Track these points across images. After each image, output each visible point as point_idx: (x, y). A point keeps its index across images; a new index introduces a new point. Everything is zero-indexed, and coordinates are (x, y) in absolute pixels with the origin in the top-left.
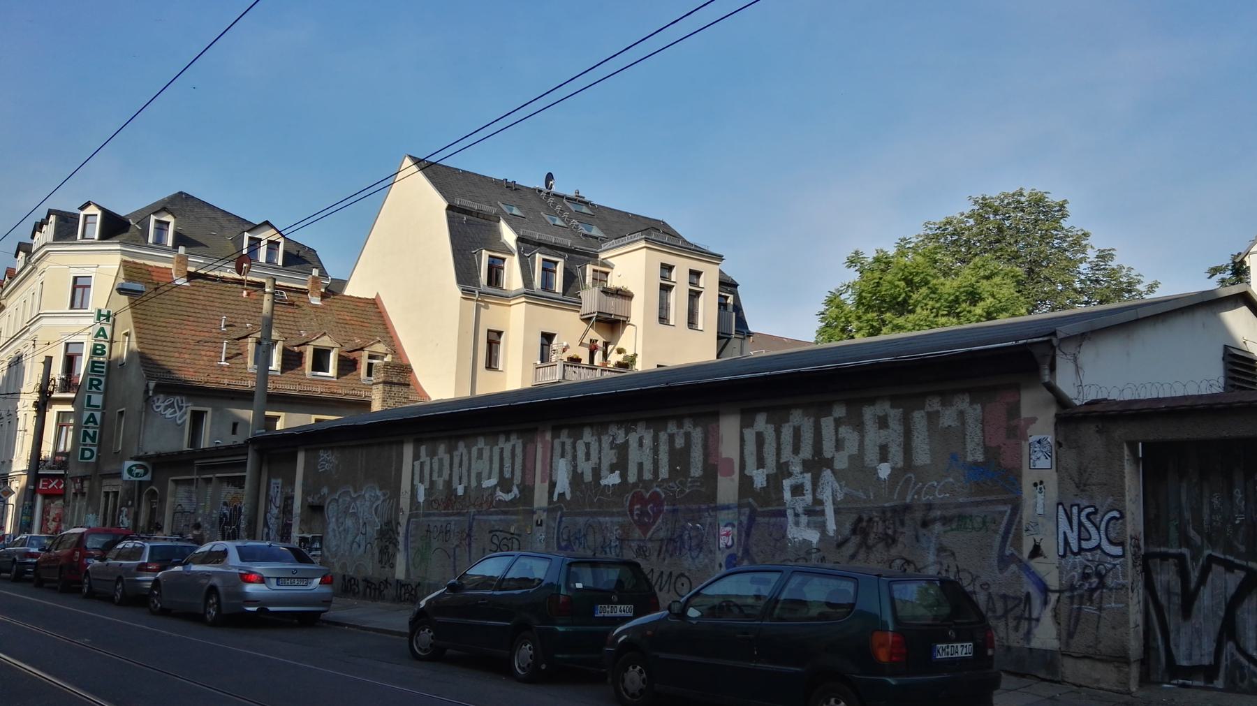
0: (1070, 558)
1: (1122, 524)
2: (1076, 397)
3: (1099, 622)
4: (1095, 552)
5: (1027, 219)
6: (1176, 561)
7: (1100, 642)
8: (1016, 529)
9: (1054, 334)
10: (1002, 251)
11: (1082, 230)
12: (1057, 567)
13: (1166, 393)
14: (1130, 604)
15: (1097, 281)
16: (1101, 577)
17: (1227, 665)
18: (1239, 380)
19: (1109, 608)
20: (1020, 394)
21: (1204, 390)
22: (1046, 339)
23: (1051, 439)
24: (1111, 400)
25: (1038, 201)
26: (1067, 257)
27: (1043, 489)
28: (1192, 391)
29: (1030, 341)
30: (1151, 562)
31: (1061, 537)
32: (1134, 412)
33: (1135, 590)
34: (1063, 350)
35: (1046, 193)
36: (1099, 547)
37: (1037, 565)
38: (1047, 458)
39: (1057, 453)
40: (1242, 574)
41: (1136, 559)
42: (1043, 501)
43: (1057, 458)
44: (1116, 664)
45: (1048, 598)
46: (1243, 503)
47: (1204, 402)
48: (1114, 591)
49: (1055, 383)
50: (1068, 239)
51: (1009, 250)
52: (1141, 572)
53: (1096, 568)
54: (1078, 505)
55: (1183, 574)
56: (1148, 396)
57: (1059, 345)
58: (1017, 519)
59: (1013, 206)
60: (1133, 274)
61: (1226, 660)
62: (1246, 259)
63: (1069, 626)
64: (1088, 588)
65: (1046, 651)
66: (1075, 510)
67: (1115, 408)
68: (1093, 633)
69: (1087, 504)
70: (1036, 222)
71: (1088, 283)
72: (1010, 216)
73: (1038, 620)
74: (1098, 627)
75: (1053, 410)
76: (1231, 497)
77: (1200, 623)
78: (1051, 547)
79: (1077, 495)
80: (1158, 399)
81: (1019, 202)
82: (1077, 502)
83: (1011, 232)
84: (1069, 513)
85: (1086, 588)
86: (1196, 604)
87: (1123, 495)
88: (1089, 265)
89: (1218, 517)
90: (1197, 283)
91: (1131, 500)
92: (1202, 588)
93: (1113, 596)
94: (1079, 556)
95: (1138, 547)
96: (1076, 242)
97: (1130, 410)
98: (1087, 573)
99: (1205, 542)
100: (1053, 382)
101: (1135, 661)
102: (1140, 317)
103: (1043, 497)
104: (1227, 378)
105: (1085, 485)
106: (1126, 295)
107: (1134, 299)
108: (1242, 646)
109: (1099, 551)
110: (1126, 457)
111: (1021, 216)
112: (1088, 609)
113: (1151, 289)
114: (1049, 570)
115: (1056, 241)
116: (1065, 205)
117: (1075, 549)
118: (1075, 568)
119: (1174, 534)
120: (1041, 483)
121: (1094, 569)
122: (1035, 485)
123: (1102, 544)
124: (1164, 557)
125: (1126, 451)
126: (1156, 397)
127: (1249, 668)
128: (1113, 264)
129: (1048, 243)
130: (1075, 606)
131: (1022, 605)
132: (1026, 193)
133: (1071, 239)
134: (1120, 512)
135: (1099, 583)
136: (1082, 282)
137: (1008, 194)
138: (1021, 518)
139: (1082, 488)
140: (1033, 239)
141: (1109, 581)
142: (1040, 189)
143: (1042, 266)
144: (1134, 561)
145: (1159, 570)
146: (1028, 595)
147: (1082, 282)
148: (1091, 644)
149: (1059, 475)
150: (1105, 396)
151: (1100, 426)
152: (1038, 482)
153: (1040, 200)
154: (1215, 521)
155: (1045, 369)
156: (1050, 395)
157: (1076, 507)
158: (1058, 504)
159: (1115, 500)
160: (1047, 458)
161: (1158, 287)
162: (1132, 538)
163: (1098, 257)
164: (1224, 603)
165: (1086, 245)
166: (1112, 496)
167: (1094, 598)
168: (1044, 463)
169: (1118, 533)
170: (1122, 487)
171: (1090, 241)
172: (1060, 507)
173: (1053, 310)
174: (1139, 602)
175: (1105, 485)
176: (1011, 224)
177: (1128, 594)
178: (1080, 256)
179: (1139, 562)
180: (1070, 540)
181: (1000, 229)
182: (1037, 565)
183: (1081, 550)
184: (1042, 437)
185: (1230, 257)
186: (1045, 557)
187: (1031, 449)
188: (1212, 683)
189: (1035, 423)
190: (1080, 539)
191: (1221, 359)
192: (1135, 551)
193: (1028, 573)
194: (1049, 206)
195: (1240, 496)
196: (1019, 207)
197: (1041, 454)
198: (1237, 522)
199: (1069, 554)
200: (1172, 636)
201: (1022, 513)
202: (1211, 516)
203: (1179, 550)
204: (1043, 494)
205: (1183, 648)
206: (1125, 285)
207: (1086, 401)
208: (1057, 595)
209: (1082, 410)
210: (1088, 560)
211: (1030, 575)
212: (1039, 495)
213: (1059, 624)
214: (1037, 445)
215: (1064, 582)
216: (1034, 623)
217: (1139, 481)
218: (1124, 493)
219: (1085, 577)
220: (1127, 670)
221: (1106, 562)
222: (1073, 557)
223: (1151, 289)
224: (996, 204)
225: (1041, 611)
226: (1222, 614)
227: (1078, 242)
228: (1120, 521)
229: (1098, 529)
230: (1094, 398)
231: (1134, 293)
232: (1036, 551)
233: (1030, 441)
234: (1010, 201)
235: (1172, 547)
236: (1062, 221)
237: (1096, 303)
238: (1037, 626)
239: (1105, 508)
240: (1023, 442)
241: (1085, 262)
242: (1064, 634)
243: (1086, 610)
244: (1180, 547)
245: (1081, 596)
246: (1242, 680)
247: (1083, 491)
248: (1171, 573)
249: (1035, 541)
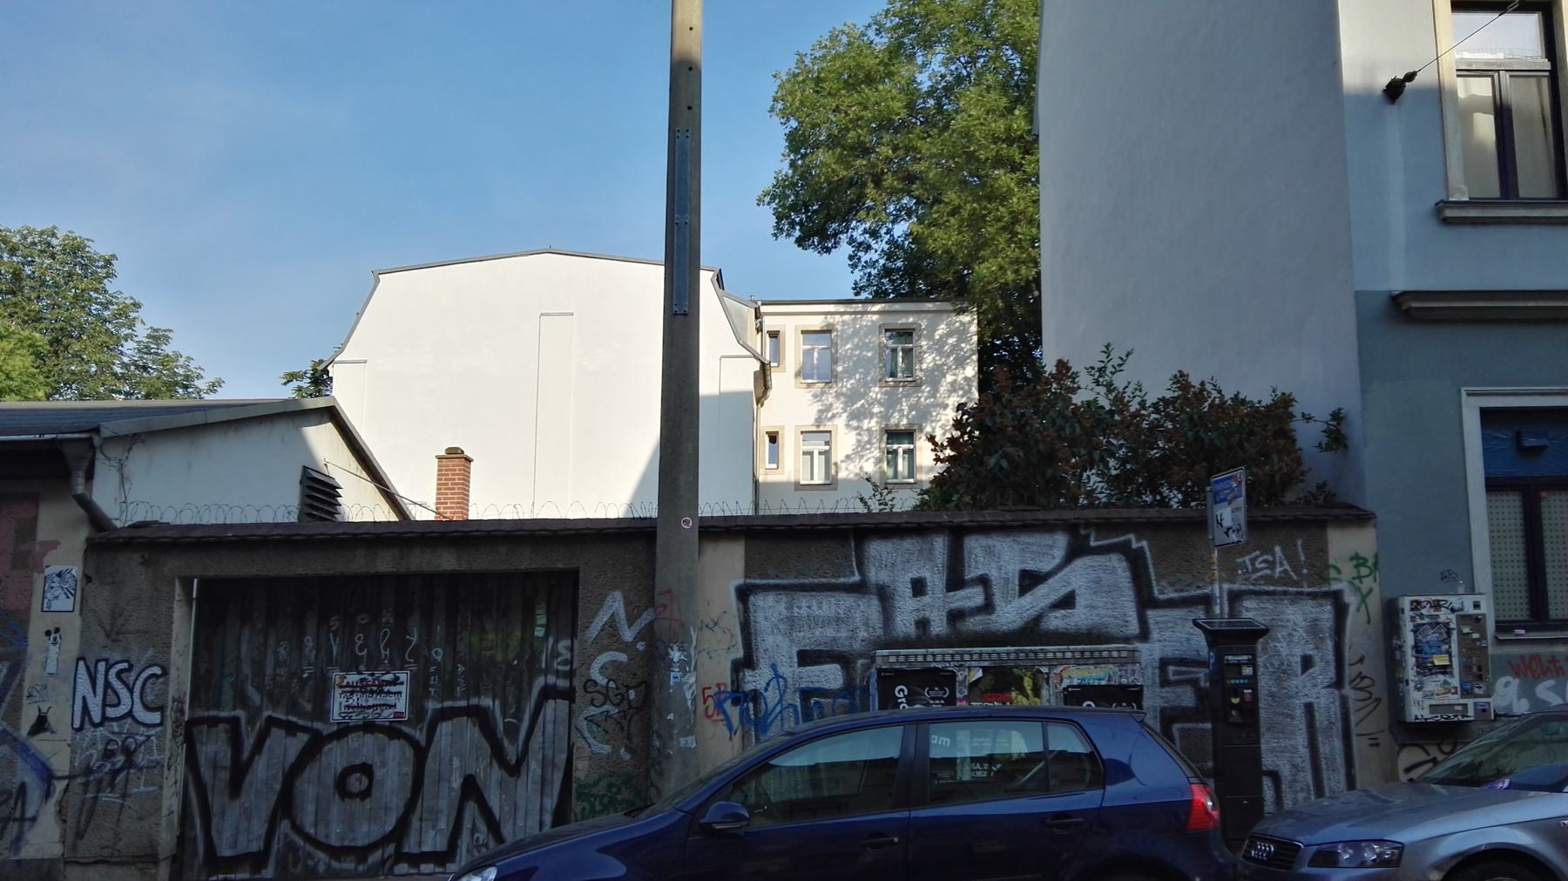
0: (89, 731)
1: (162, 683)
2: (116, 517)
3: (120, 814)
4: (124, 721)
5: (57, 270)
6: (227, 727)
7: (120, 840)
8: (12, 696)
9: (97, 430)
10: (15, 307)
11: (132, 298)
12: (69, 746)
13: (235, 518)
14: (165, 786)
15: (145, 368)
16: (129, 753)
17: (279, 849)
18: (317, 509)
19: (135, 793)
20: (37, 508)
21: (281, 518)
22: (84, 436)
23: (76, 572)
24: (162, 523)
25: (75, 249)
26: (107, 330)
27: (58, 639)
28: (267, 518)
29: (60, 436)
30: (195, 730)
31: (79, 703)
32: (572, 532)
33: (173, 767)
34: (105, 453)
35: (87, 240)
36: (130, 714)
37: (41, 744)
38: (68, 597)
39: (83, 590)
40: (304, 738)
41: (177, 727)
42: (57, 656)
43: (82, 598)
44: (140, 865)
45: (52, 788)
46: (314, 652)
47: (280, 532)
48: (145, 770)
49: (91, 496)
50: (111, 307)
51: (28, 308)
52: (182, 744)
53: (123, 742)
54: (106, 660)
55: (236, 741)
56: (213, 521)
57: (101, 447)
58: (17, 681)
59: (39, 247)
60: (192, 365)
61: (279, 843)
62: (329, 368)
63: (79, 822)
64: (110, 770)
65: (42, 860)
66: (102, 666)
67: (169, 533)
68: (112, 829)
69: (118, 658)
70: (69, 276)
71: (132, 368)
72: (33, 261)
73: (34, 819)
74: (118, 820)
75: (84, 533)
76: (300, 646)
77: (251, 802)
78: (62, 717)
79: (105, 647)
80: (225, 525)
81: (49, 244)
82: (104, 656)
83: (32, 283)
84: (92, 670)
85: (107, 770)
86: (249, 778)
87: (169, 647)
88: (135, 345)
89: (282, 671)
90: (274, 390)
91: (178, 652)
92: (257, 757)
93: (143, 777)
94: (101, 728)
95: (182, 711)
96: (122, 313)
97: (187, 537)
98: (110, 750)
99: (265, 700)
100: (88, 495)
101: (165, 859)
102: (209, 421)
103: (57, 650)
104: (303, 504)
105: (118, 633)
106: (181, 391)
107: (189, 397)
108: (298, 823)
109: (129, 720)
110: (177, 598)
111: (50, 265)
112: (107, 797)
113: (213, 388)
114: (58, 752)
115: (95, 306)
116: (113, 262)
117: (97, 719)
118: (94, 744)
119: (228, 694)
120: (57, 630)
121: (120, 743)
122: (48, 633)
123: (134, 710)
124: (213, 722)
125: (178, 590)
126: (221, 522)
127: (304, 848)
128: (168, 349)
129: (83, 307)
130: (90, 795)
131: (12, 802)
132: (61, 234)
133: (115, 307)
134: (163, 668)
135: (126, 762)
136: (124, 365)
137: (34, 230)
138: (22, 680)
139: (114, 636)
140: (64, 298)
141: (140, 759)
142: (80, 232)
143: (72, 337)
144: (174, 731)
145: (205, 738)
146: (23, 788)
147: (124, 365)
148: (108, 843)
149: (83, 621)
150: (156, 517)
151: (146, 556)
152: (52, 630)
153: (78, 248)
154: (278, 675)
155: (79, 476)
156: (81, 511)
157: (103, 663)
158: (78, 659)
159: (157, 653)
160: (68, 597)
161: (220, 386)
162: (174, 700)
163: (149, 336)
164: (281, 774)
165: (135, 318)
166: (154, 647)
167: (116, 782)
168: (65, 603)
169: (157, 695)
170: (169, 635)
171: (141, 314)
172: (81, 663)
173: (82, 396)
174: (176, 783)
175: (146, 633)
176: (34, 272)
177: (162, 773)
178: (125, 331)
179: (181, 730)
180: (91, 707)
181: (17, 276)
182: (41, 744)
183: (105, 719)
184: (63, 568)
185: (311, 364)
186: (53, 732)
187: (47, 584)
188: (259, 872)
189: (56, 548)
190: (105, 705)
191: (298, 482)
192: (177, 718)
193: (24, 755)
194: (90, 259)
195: (311, 645)
196: (48, 250)
197: (60, 591)
198: (305, 676)
199: (87, 726)
200: (215, 820)
201: (24, 672)
202: (275, 669)
203: (233, 713)
204: (57, 646)
205: (227, 835)
206: (179, 378)
207: (130, 523)
208: (66, 782)
209: (125, 534)
210: (113, 733)
211: (28, 760)
212: (52, 647)
213: (65, 821)
214: (56, 579)
215: (76, 764)
216: (27, 824)
217: (190, 628)
218: (170, 643)
219: (108, 754)
220: (153, 871)
221: (137, 734)
222: (92, 729)
223: (213, 388)
224: (14, 240)
225: (40, 806)
226: (278, 787)
227: (126, 313)
228: (161, 680)
229: (131, 691)
230: (143, 520)
231: (190, 390)
232: (41, 725)
233: (46, 574)
234: (36, 240)
235: (223, 711)
236: (105, 281)
237: (139, 396)
238: (31, 827)
239: (142, 663)
240: (36, 575)
241: (132, 340)
242: (70, 834)
243: (104, 799)
244: (234, 709)
245: (100, 782)
246: (295, 865)
247: (115, 641)
248: (219, 743)
249: (40, 710)
